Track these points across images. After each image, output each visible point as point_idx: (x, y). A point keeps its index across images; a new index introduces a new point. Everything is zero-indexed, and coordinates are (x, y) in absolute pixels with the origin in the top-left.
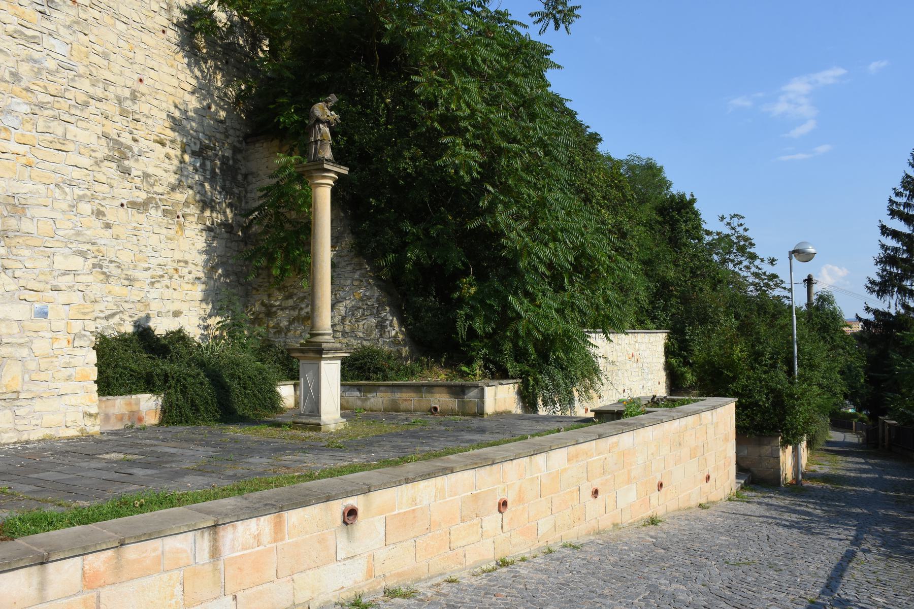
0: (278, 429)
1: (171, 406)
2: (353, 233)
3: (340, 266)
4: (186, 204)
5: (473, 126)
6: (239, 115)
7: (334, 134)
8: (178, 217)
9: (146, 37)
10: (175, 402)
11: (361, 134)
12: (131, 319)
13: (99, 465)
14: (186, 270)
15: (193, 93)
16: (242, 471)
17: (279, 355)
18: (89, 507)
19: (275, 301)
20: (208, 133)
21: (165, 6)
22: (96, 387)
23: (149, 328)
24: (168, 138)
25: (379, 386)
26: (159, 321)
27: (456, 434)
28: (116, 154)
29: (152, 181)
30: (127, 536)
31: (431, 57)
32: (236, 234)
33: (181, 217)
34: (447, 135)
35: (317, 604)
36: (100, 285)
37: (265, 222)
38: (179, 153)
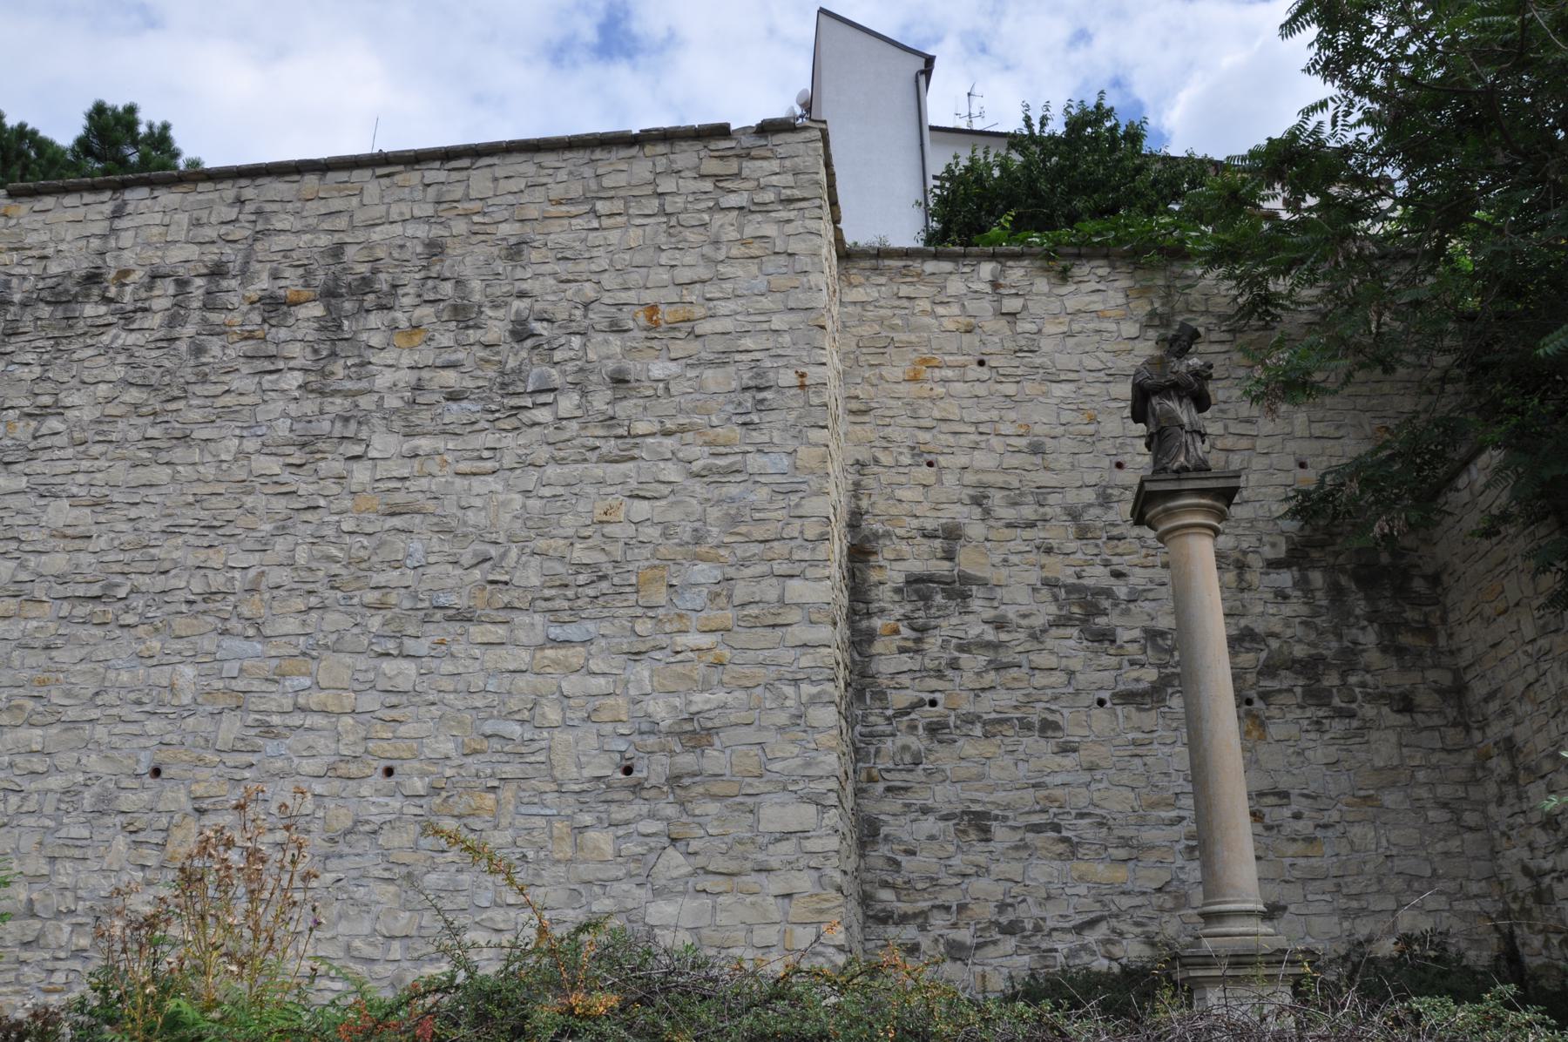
28: (1075, 609)
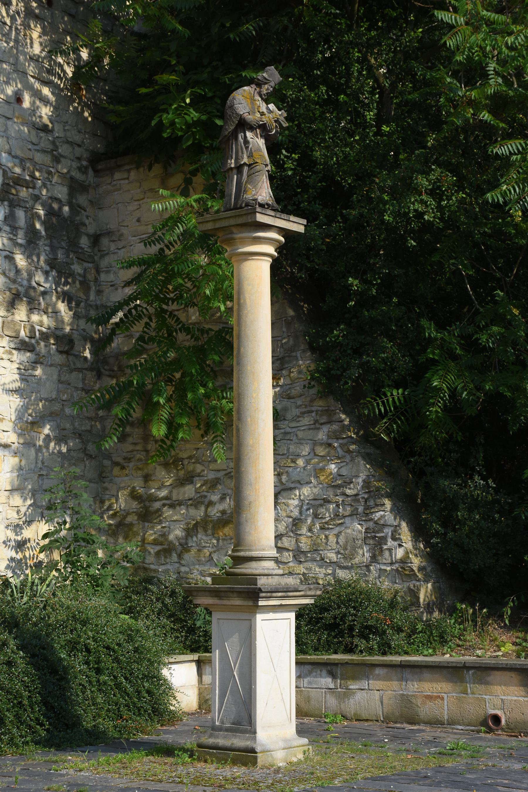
0: (169, 760)
2: (312, 348)
3: (289, 416)
11: (327, 148)
17: (168, 601)
19: (159, 489)
20: (19, 153)
25: (374, 666)
32: (79, 357)
34: (509, 136)
37: (138, 329)
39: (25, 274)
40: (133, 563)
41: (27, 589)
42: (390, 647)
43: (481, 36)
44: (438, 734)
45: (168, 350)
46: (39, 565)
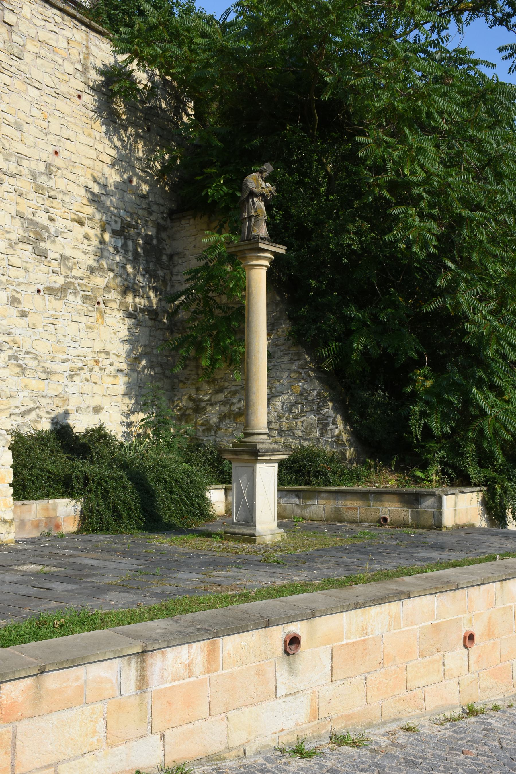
0: (210, 539)
1: (91, 511)
2: (290, 318)
3: (276, 356)
4: (107, 289)
5: (429, 193)
6: (162, 188)
7: (268, 207)
8: (98, 303)
9: (61, 104)
10: (95, 507)
11: (299, 207)
12: (48, 416)
13: (15, 578)
14: (108, 362)
15: (112, 165)
16: (170, 588)
17: (209, 456)
18: (5, 627)
19: (204, 395)
20: (130, 210)
21: (80, 68)
22: (11, 491)
23: (68, 426)
24: (85, 216)
25: (321, 492)
26: (78, 418)
27: (410, 550)
29: (70, 264)
30: (48, 662)
31: (379, 114)
32: (161, 322)
33: (101, 303)
34: (398, 204)
35: (254, 749)
36: (15, 378)
37: (193, 307)
38: (98, 231)
39: (132, 276)
40: (190, 435)
41: (133, 448)
42: (329, 482)
43: (381, 150)
44: (354, 527)
45: (210, 319)
46: (139, 436)
